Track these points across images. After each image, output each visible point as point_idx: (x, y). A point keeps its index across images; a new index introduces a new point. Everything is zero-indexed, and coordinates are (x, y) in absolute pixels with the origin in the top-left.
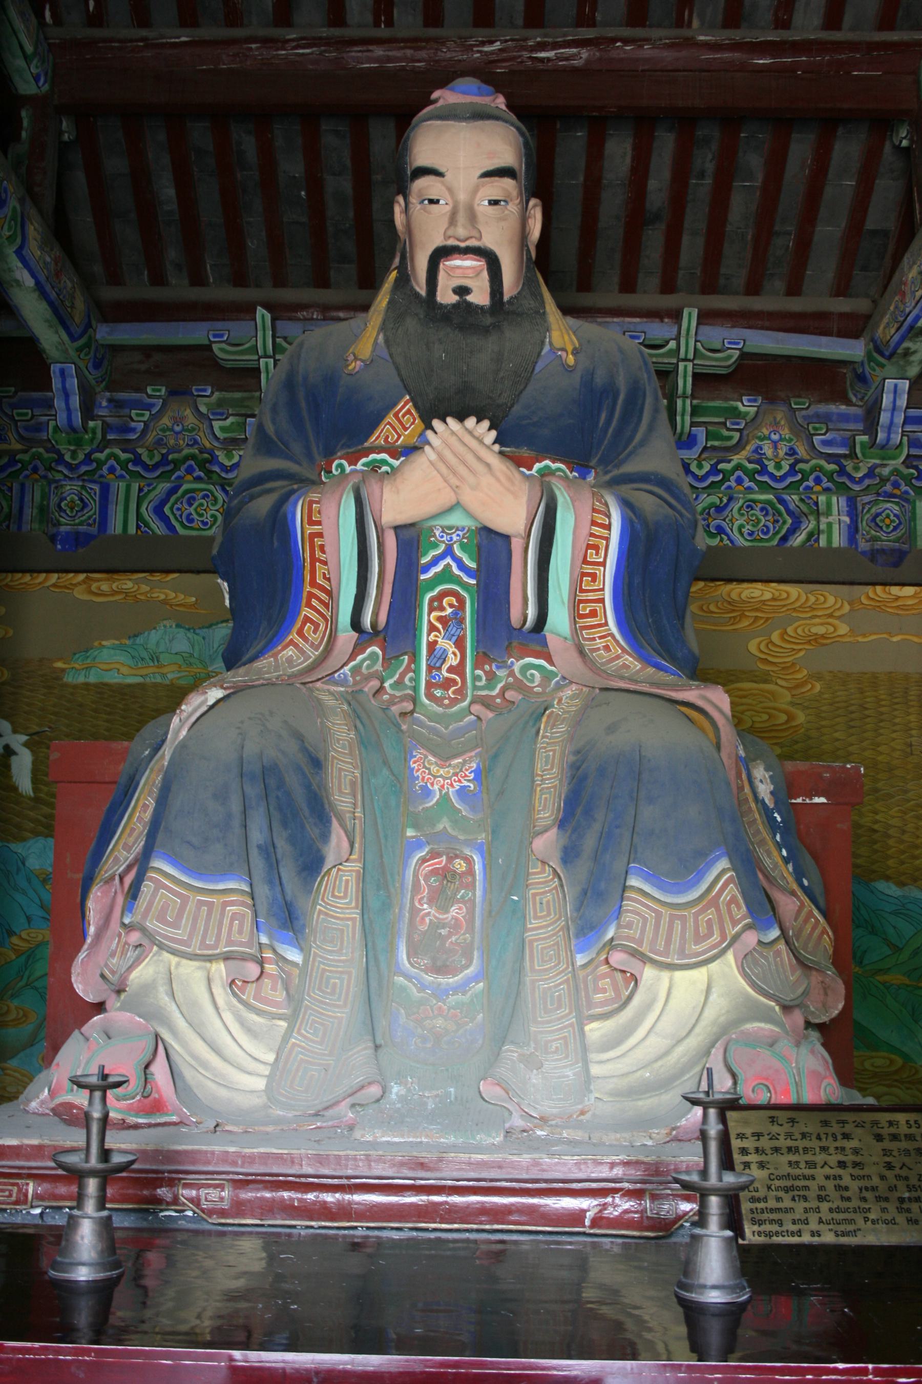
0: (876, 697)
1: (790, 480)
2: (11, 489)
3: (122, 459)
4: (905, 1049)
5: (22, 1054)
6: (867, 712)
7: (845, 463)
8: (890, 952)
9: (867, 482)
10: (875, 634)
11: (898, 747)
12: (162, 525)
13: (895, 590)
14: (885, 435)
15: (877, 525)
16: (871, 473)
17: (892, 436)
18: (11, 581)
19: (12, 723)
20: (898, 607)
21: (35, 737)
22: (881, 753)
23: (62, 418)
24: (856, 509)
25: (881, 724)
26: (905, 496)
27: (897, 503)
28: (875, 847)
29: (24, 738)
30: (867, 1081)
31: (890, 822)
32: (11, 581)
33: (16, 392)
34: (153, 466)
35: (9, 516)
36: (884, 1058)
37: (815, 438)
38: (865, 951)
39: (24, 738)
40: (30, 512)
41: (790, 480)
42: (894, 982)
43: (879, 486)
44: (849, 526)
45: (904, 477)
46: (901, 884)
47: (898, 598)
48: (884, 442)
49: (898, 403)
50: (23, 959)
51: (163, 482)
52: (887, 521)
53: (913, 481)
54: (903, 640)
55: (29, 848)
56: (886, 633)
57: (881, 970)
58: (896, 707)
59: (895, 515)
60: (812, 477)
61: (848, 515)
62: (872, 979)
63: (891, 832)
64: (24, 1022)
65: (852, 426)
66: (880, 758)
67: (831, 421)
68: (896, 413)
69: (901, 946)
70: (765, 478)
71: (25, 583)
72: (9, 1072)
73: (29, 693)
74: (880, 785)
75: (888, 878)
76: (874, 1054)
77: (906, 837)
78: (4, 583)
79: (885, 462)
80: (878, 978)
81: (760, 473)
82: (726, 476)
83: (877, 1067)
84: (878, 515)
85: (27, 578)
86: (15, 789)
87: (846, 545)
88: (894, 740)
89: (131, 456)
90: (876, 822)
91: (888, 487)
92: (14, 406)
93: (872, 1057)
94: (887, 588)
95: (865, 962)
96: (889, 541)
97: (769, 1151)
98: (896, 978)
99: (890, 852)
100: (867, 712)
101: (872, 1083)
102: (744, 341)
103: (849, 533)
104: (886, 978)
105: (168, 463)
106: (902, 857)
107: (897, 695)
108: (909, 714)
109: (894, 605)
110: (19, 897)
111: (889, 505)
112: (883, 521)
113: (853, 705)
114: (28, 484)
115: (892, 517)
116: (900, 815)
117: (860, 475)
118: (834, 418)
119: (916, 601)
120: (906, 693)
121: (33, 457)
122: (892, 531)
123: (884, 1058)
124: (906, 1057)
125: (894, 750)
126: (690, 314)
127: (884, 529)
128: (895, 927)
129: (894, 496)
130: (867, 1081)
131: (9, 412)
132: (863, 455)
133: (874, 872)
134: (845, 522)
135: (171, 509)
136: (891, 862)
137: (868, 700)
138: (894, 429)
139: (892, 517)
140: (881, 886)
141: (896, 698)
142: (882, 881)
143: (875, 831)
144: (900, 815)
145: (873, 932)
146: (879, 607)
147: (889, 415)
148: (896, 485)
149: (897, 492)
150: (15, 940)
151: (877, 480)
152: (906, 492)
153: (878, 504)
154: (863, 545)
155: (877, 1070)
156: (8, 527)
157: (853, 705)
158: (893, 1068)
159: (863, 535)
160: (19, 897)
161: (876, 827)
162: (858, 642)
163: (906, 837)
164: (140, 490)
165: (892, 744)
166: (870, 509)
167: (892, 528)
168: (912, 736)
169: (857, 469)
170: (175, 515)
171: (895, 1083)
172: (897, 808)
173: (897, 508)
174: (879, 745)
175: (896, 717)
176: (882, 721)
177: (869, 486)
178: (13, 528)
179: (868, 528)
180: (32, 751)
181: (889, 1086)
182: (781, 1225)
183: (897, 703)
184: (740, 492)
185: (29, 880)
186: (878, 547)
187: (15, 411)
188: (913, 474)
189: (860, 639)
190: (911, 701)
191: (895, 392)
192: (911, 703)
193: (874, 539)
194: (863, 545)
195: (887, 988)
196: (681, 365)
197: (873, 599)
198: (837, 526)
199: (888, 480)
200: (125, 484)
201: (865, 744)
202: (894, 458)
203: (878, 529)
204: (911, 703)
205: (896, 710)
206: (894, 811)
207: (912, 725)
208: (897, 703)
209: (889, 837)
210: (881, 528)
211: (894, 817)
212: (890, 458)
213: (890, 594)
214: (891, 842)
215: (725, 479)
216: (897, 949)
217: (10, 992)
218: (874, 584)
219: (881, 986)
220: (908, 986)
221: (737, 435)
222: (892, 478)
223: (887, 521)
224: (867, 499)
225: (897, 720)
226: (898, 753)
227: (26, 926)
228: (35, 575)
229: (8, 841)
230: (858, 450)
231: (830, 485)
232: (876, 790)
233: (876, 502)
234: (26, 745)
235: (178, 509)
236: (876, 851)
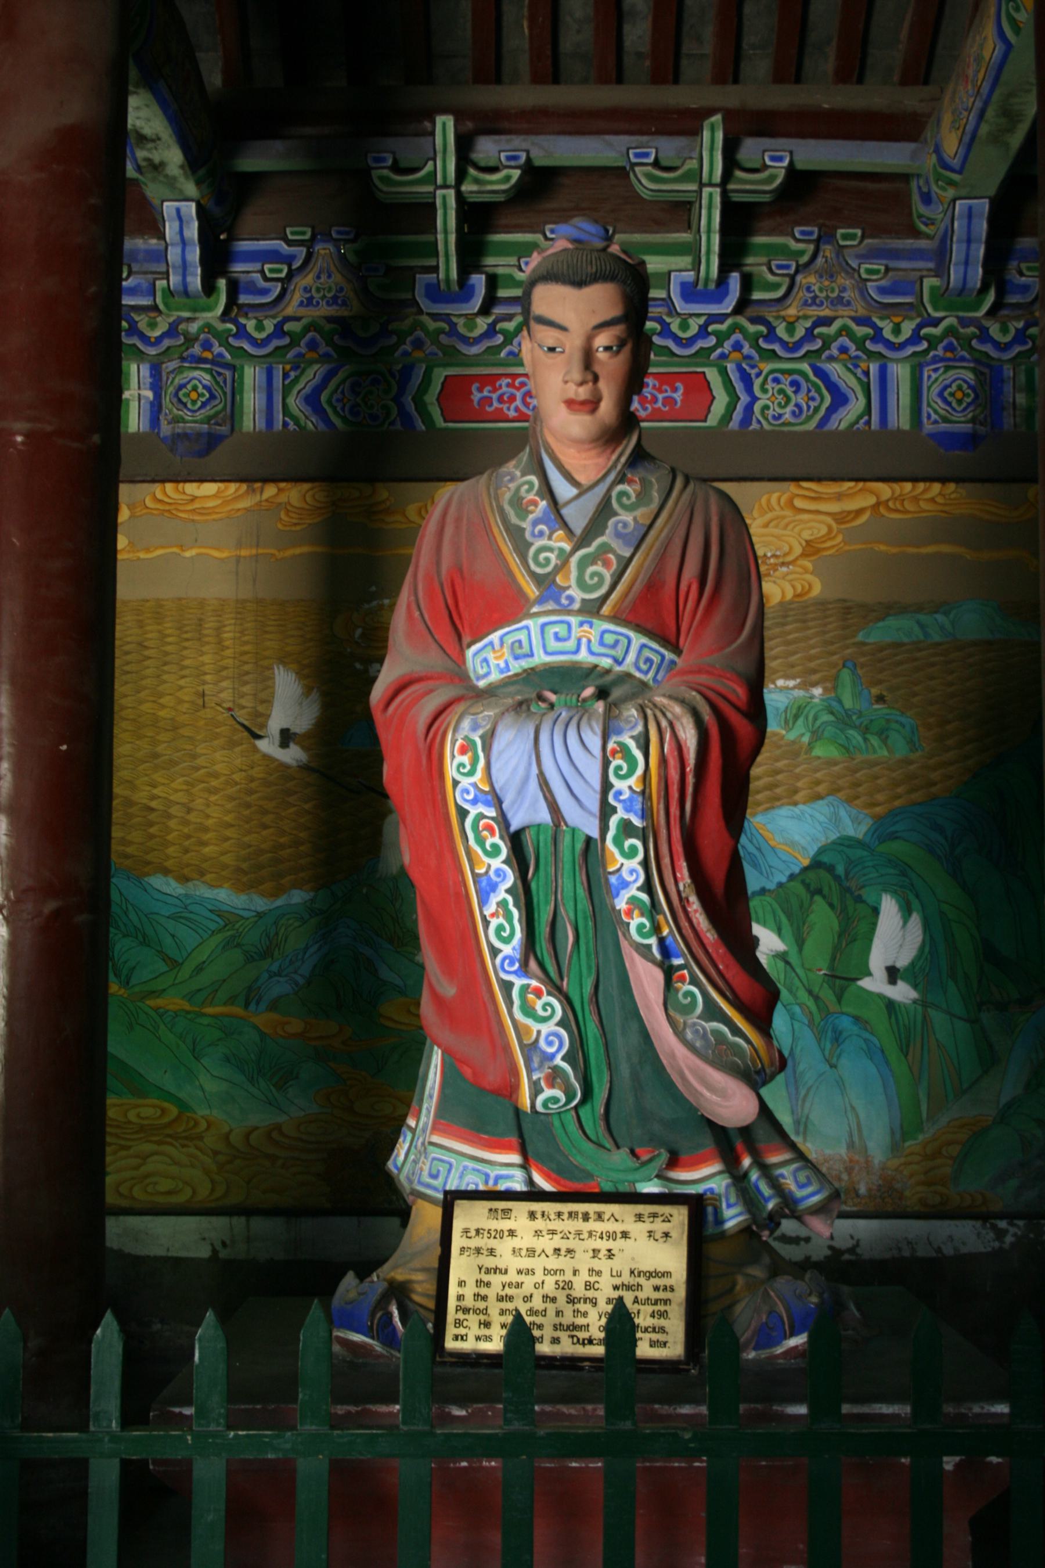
0: (159, 632)
1: (276, 343)
3: (859, 335)
4: (181, 1095)
6: (147, 653)
7: (137, 318)
8: (165, 968)
9: (167, 343)
10: (163, 547)
11: (186, 698)
13: (191, 488)
14: (179, 278)
15: (180, 401)
16: (172, 331)
17: (189, 279)
20: (191, 511)
22: (163, 707)
24: (160, 379)
25: (166, 668)
26: (219, 359)
27: (210, 371)
28: (152, 830)
30: (133, 1137)
31: (172, 798)
34: (262, 340)
36: (154, 1106)
37: (869, 284)
38: (134, 968)
42: (171, 1007)
43: (183, 348)
44: (152, 404)
45: (217, 334)
46: (184, 879)
47: (194, 499)
48: (960, 285)
49: (187, 234)
52: (194, 396)
53: (231, 340)
54: (198, 555)
56: (177, 546)
57: (154, 992)
58: (186, 644)
59: (205, 387)
61: (151, 389)
62: (140, 1004)
63: (174, 810)
65: (920, 264)
66: (162, 713)
67: (136, 260)
68: (188, 249)
69: (180, 961)
74: (160, 749)
75: (166, 872)
76: (141, 1101)
77: (192, 817)
79: (198, 315)
80: (148, 1002)
81: (236, 336)
83: (142, 1118)
84: (181, 387)
87: (147, 429)
88: (181, 688)
89: (870, 331)
90: (154, 797)
91: (197, 349)
93: (138, 1106)
94: (181, 485)
95: (133, 982)
96: (195, 422)
97: (552, 1217)
98: (173, 1002)
99: (169, 838)
100: (147, 653)
101: (140, 1139)
102: (791, 153)
103: (152, 412)
104: (160, 1002)
106: (187, 843)
107: (188, 628)
108: (203, 654)
109: (190, 507)
111: (196, 373)
112: (188, 395)
113: (128, 643)
115: (200, 389)
116: (185, 787)
117: (157, 333)
118: (141, 256)
119: (219, 502)
120: (201, 625)
122: (200, 408)
123: (154, 1106)
124: (183, 1106)
125: (181, 701)
126: (444, 124)
127: (189, 406)
128: (173, 936)
129: (205, 361)
130: (133, 1137)
132: (166, 304)
133: (149, 863)
134: (147, 398)
136: (171, 850)
137: (149, 636)
138: (190, 270)
139: (200, 389)
140: (157, 881)
141: (186, 632)
142: (159, 875)
143: (152, 810)
144: (185, 787)
145: (145, 941)
146: (169, 511)
147: (179, 250)
148: (207, 346)
149: (208, 355)
151: (182, 340)
152: (220, 355)
153: (182, 372)
154: (166, 429)
155: (146, 1122)
157: (128, 643)
158: (166, 1120)
159: (166, 414)
161: (154, 804)
162: (139, 559)
163: (192, 817)
164: (286, 375)
165: (179, 694)
166: (174, 379)
167: (199, 403)
168: (204, 683)
169: (153, 325)
170: (334, 408)
171: (169, 1140)
172: (181, 780)
173: (208, 377)
174: (161, 695)
175: (185, 658)
176: (165, 664)
177: (169, 348)
179: (170, 406)
181: (159, 1143)
183: (187, 640)
186: (180, 431)
188: (231, 330)
189: (142, 555)
190: (169, 636)
191: (970, 216)
192: (207, 639)
193: (176, 420)
194: (166, 429)
195: (161, 1016)
196: (439, 192)
197: (160, 501)
198: (137, 403)
199: (196, 339)
200: (877, 365)
201: (142, 695)
202: (209, 309)
203: (181, 406)
204: (207, 639)
205: (185, 648)
206: (179, 783)
207: (207, 668)
208: (187, 640)
209: (170, 817)
210: (185, 405)
211: (176, 791)
212: (203, 310)
213: (184, 493)
214: (172, 824)
216: (174, 964)
218: (163, 481)
219: (153, 1013)
220: (188, 1012)
222: (202, 336)
223: (194, 396)
224: (172, 365)
225: (187, 662)
226: (186, 705)
230: (159, 300)
231: (222, 350)
232: (156, 756)
233: (179, 370)
235: (813, 399)
236: (152, 837)
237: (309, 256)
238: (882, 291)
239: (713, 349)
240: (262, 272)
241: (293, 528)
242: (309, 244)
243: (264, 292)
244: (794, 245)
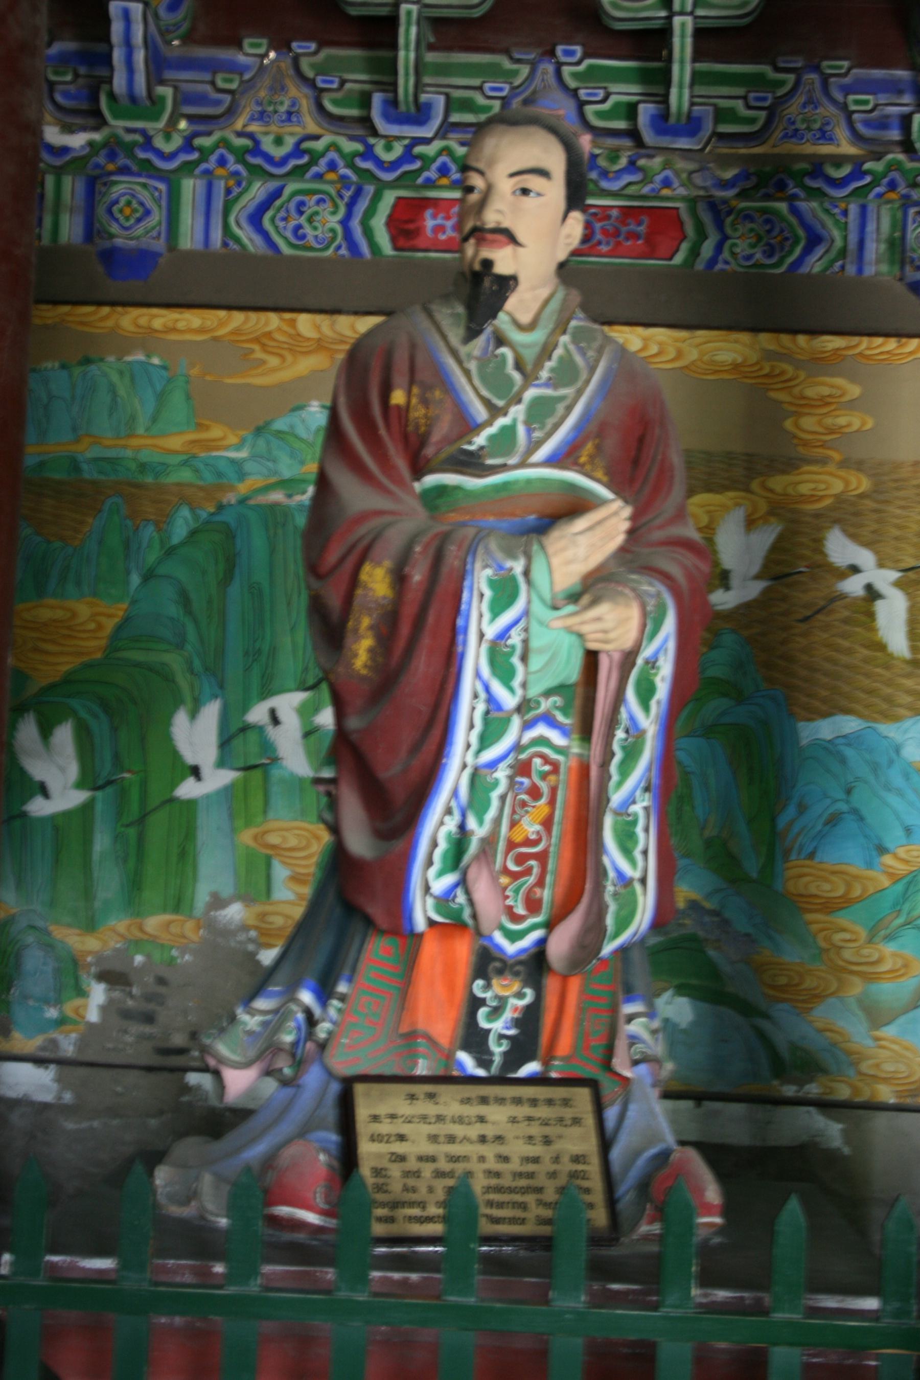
1: (293, 163)
2: (845, 213)
5: (902, 1020)
12: (258, 239)
18: (868, 349)
19: (876, 553)
21: (911, 575)
23: (119, 82)
29: (895, 575)
32: (868, 349)
33: (849, 69)
34: (391, 163)
35: (843, 253)
39: (895, 575)
40: (874, 249)
41: (293, 163)
50: (900, 887)
51: (294, 181)
52: (128, 211)
55: (905, 732)
60: (213, 158)
64: (902, 975)
70: (257, 161)
71: (888, 352)
72: (883, 1043)
73: (898, 511)
78: (857, 351)
82: (204, 154)
85: (891, 344)
86: (881, 647)
92: (847, 90)
105: (413, 158)
110: (893, 800)
114: (872, 207)
115: (135, 205)
121: (890, 167)
131: (839, 97)
135: (273, 220)
150: (888, 860)
156: (843, 267)
160: (893, 800)
164: (228, 191)
170: (276, 227)
178: (851, 270)
180: (908, 594)
182: (424, 1208)
184: (221, 178)
185: (907, 776)
187: (851, 97)
193: (726, 262)
215: (203, 159)
217: (883, 933)
221: (763, 114)
227: (904, 841)
228: (904, 340)
229: (875, 720)
231: (240, 167)
234: (898, 584)
237: (797, 83)
238: (600, 115)
239: (197, 163)
240: (213, 83)
241: (709, 377)
242: (534, 65)
243: (218, 103)
244: (507, 64)
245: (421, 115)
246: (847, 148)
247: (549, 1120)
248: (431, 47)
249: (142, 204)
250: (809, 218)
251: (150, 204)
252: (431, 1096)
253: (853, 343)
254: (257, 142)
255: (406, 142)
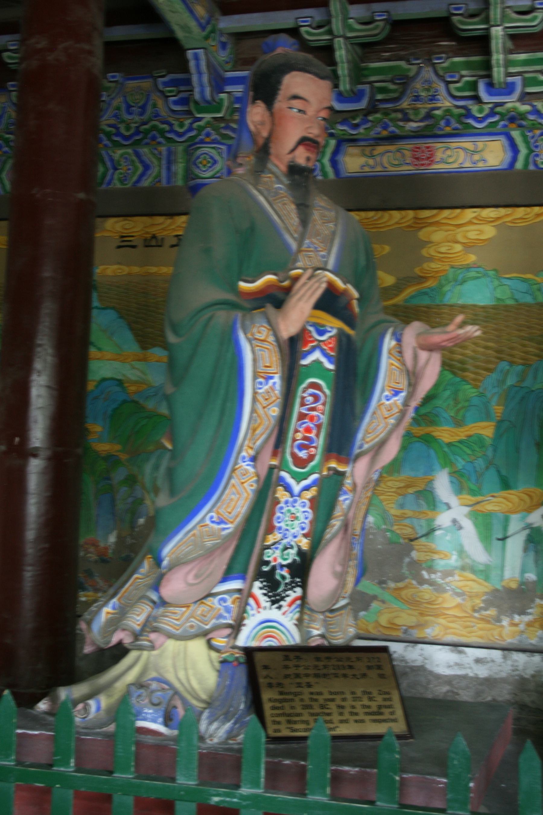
52: (205, 162)
238: (458, 89)
245: (509, 89)
246: (446, 103)
247: (352, 678)
248: (511, 52)
249: (212, 158)
250: (145, 158)
251: (217, 157)
252: (298, 658)
253: (509, 212)
254: (118, 129)
255: (490, 106)
